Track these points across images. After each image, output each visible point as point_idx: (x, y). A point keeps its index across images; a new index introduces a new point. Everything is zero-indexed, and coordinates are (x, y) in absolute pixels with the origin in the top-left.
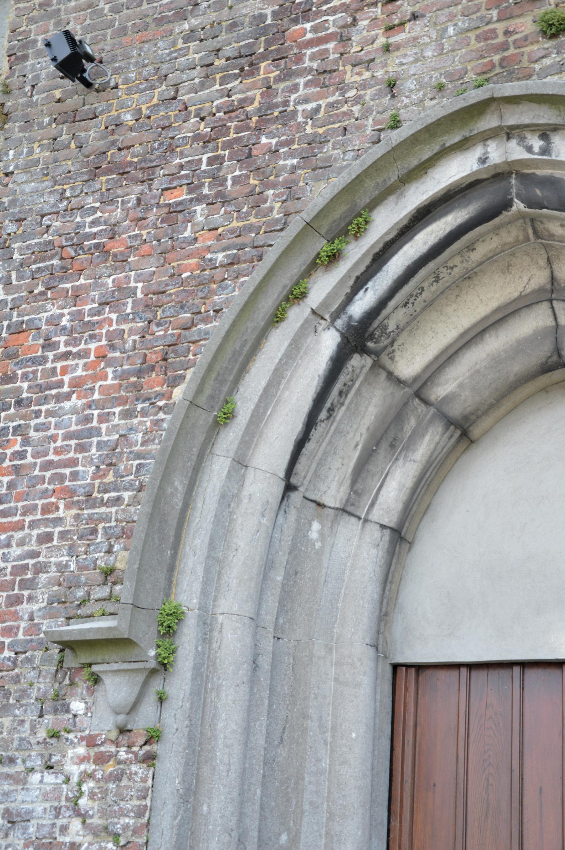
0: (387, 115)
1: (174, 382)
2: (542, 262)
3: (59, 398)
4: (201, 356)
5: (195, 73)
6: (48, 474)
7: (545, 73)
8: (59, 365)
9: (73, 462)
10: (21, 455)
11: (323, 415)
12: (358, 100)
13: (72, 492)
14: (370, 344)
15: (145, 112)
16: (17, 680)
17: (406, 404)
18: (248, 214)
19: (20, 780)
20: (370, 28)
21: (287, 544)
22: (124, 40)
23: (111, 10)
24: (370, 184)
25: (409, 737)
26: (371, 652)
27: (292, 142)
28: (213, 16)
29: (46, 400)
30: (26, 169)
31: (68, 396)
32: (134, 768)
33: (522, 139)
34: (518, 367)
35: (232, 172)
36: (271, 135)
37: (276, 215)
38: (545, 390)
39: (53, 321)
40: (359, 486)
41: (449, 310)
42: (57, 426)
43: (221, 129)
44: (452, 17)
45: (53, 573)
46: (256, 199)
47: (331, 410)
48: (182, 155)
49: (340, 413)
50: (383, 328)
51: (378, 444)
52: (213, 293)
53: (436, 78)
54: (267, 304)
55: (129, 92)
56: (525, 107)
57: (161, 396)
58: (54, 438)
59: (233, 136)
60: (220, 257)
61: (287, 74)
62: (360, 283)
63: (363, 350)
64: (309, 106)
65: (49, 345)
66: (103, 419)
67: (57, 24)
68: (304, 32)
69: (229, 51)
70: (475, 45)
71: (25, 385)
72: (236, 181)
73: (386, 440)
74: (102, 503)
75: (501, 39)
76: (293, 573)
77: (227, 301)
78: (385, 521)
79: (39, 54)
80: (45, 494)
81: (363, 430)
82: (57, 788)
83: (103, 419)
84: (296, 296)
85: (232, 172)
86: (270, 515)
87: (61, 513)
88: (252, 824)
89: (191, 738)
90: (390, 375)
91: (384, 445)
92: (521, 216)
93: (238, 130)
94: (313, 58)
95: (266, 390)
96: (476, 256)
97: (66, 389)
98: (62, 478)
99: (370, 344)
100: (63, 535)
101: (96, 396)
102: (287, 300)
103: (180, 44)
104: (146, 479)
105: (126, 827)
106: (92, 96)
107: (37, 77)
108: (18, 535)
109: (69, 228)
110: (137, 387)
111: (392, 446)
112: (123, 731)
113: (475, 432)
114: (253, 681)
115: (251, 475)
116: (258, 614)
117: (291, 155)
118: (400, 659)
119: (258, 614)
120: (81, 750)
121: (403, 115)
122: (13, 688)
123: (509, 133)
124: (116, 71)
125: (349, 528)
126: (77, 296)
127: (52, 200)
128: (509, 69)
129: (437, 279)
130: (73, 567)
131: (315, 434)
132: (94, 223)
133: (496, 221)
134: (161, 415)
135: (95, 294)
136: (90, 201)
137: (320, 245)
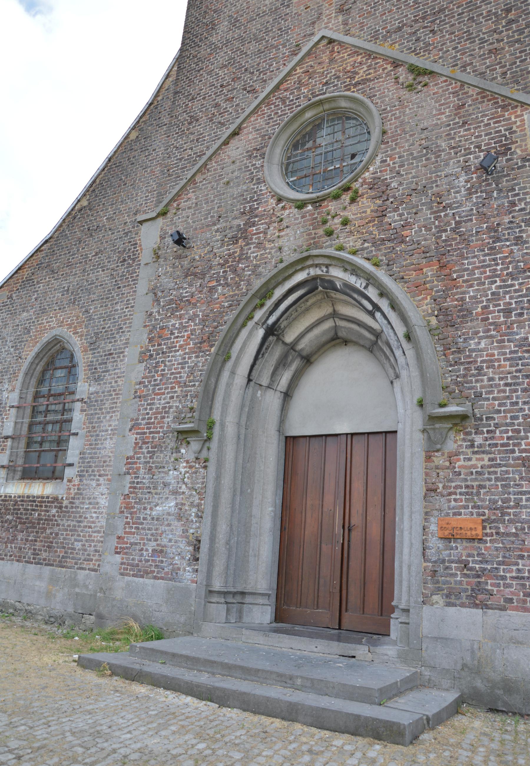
0: (279, 258)
1: (212, 346)
2: (331, 305)
3: (176, 351)
4: (220, 337)
5: (218, 243)
6: (172, 377)
7: (326, 247)
8: (175, 340)
9: (180, 373)
10: (164, 370)
11: (260, 356)
12: (270, 253)
13: (179, 383)
14: (276, 333)
15: (203, 255)
16: (164, 442)
17: (288, 352)
18: (235, 290)
19: (167, 473)
20: (273, 230)
21: (249, 398)
22: (196, 232)
23: (193, 222)
24: (273, 281)
25: (291, 459)
26: (277, 433)
27: (249, 266)
28: (224, 224)
29: (171, 352)
30: (165, 274)
31: (178, 351)
32: (201, 470)
33: (320, 268)
34: (324, 339)
35: (230, 276)
36: (242, 264)
37: (244, 290)
38: (334, 346)
39: (174, 325)
40: (273, 379)
41: (302, 320)
42: (175, 360)
43: (227, 262)
44: (298, 228)
45: (174, 409)
46: (238, 285)
47: (263, 354)
48: (214, 270)
49: (266, 355)
50: (279, 327)
51: (279, 365)
52: (224, 316)
53: (294, 247)
54: (241, 321)
55: (197, 249)
56: (320, 258)
57: (208, 351)
58: (174, 365)
59: (231, 263)
60: (226, 304)
61: (248, 244)
62: (271, 313)
63: (273, 335)
64: (255, 255)
65: (172, 333)
66: (189, 358)
67: (175, 227)
68: (253, 230)
69: (229, 236)
70: (306, 237)
71: (165, 347)
72: (231, 279)
73: (282, 363)
74: (189, 386)
75: (313, 235)
76: (251, 408)
77: (228, 319)
78: (282, 390)
79: (169, 237)
80: (171, 383)
81: (275, 360)
82: (178, 476)
83: (189, 358)
84: (250, 318)
85: (230, 276)
86: (243, 389)
87: (176, 389)
88: (238, 487)
89: (218, 461)
90: (283, 342)
91: (281, 365)
92: (321, 291)
93: (232, 262)
94: (256, 239)
95: (241, 349)
96: (309, 303)
97: (177, 348)
98: (176, 378)
99: (276, 333)
100: (177, 397)
101: (187, 351)
102: (247, 319)
103: (214, 233)
104: (202, 378)
105: (199, 487)
106: (186, 250)
107: (169, 244)
108: (163, 396)
109: (178, 294)
110: (200, 348)
111: (284, 366)
112: (197, 459)
113: (312, 360)
114: (238, 443)
115: (236, 377)
116: (239, 422)
117: (249, 271)
118: (288, 435)
119: (239, 422)
120: (185, 464)
121: (284, 258)
122: (163, 445)
123: (317, 266)
124: (194, 242)
125: (270, 392)
126: (181, 317)
127: (173, 285)
128: (317, 246)
129: (297, 311)
130: (180, 407)
131: (258, 363)
132: (186, 293)
133: (314, 293)
134: (208, 357)
135: (187, 316)
136: (185, 286)
137: (257, 301)
